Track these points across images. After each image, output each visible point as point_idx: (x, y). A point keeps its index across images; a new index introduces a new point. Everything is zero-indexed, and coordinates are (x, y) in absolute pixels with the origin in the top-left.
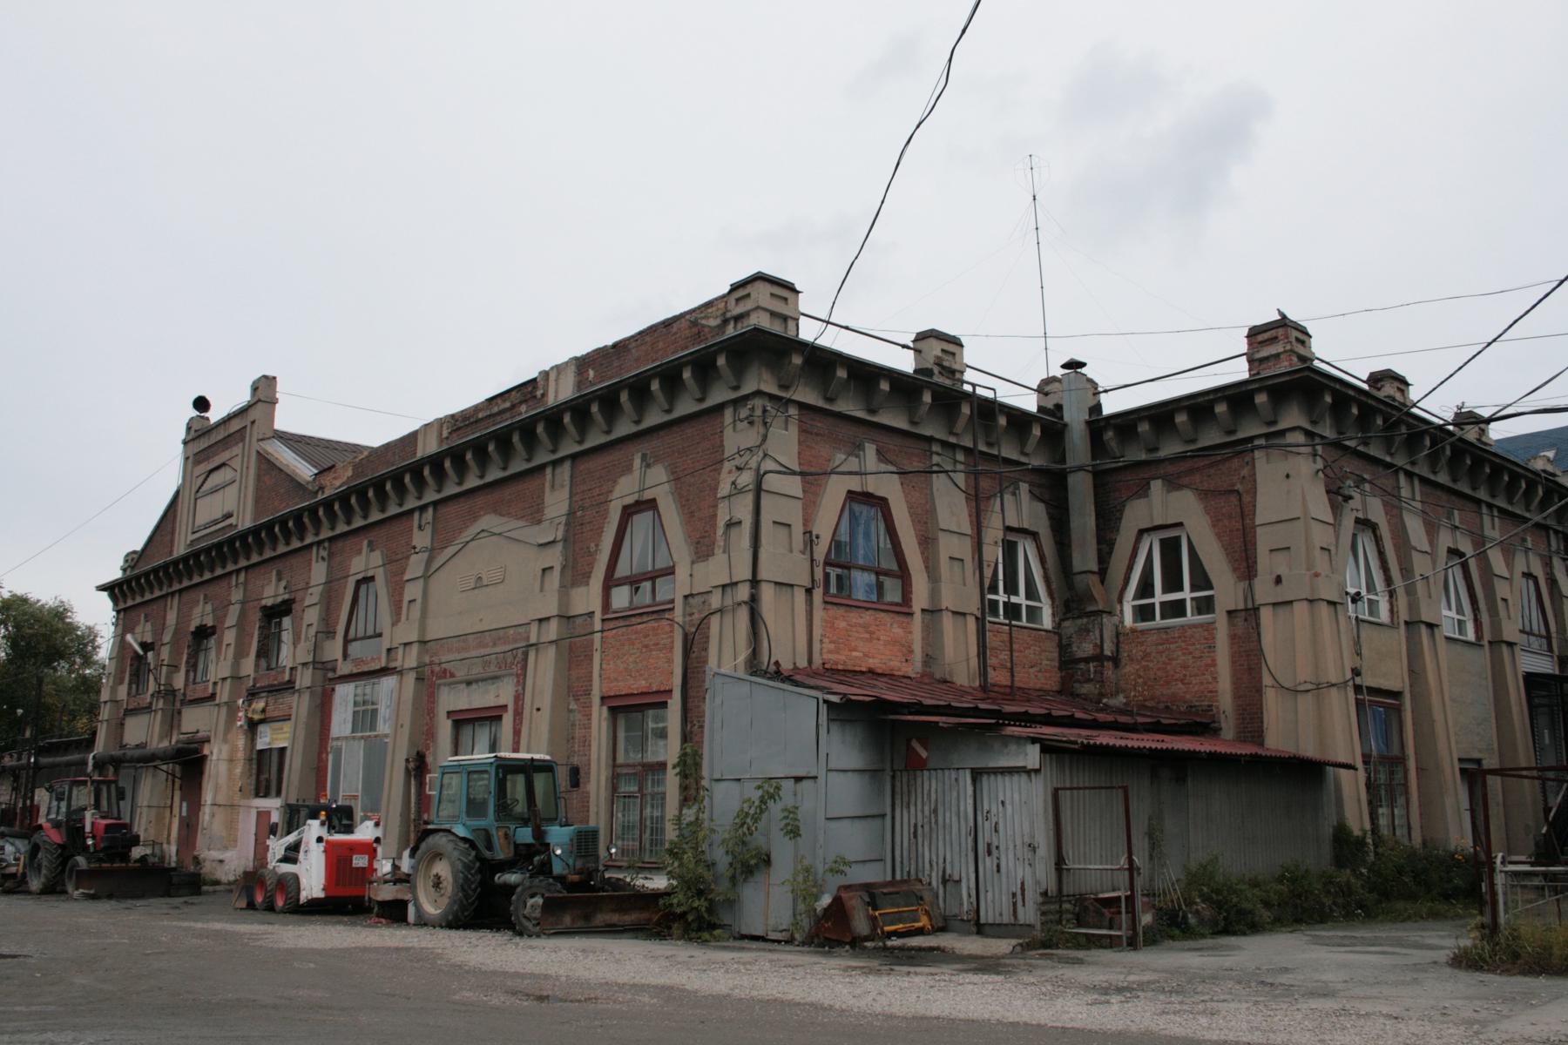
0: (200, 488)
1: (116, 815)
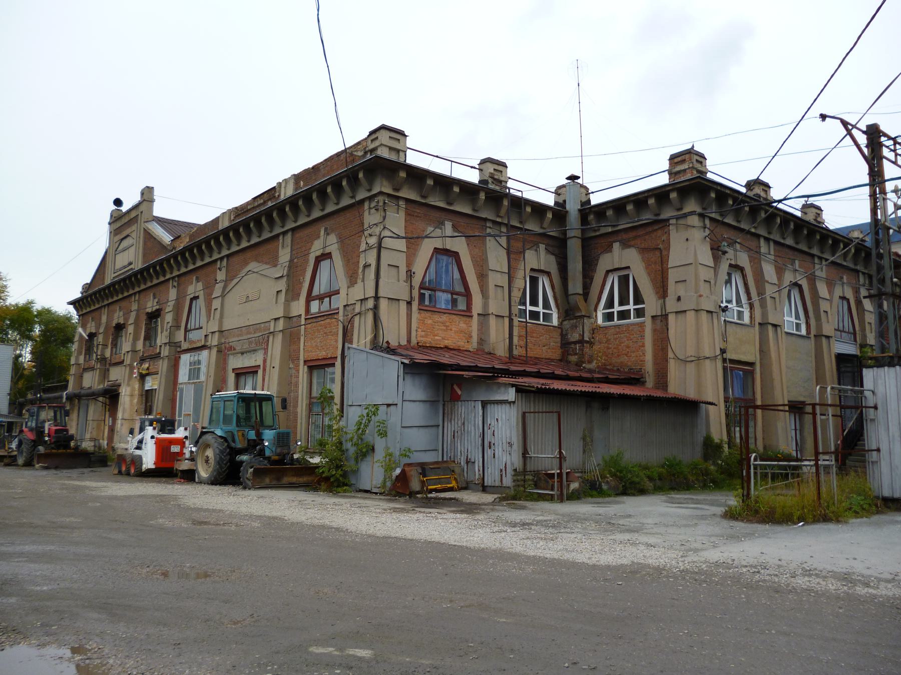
0: (117, 248)
1: (64, 425)
